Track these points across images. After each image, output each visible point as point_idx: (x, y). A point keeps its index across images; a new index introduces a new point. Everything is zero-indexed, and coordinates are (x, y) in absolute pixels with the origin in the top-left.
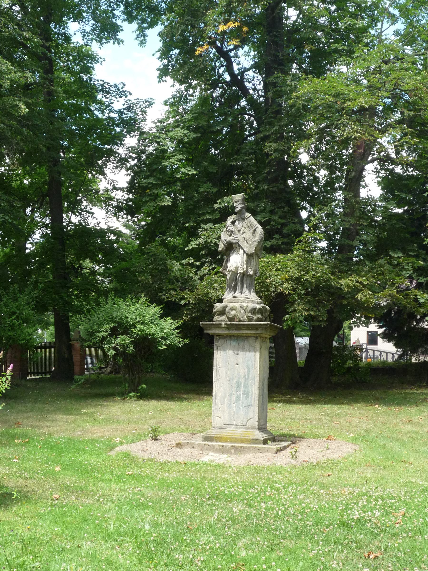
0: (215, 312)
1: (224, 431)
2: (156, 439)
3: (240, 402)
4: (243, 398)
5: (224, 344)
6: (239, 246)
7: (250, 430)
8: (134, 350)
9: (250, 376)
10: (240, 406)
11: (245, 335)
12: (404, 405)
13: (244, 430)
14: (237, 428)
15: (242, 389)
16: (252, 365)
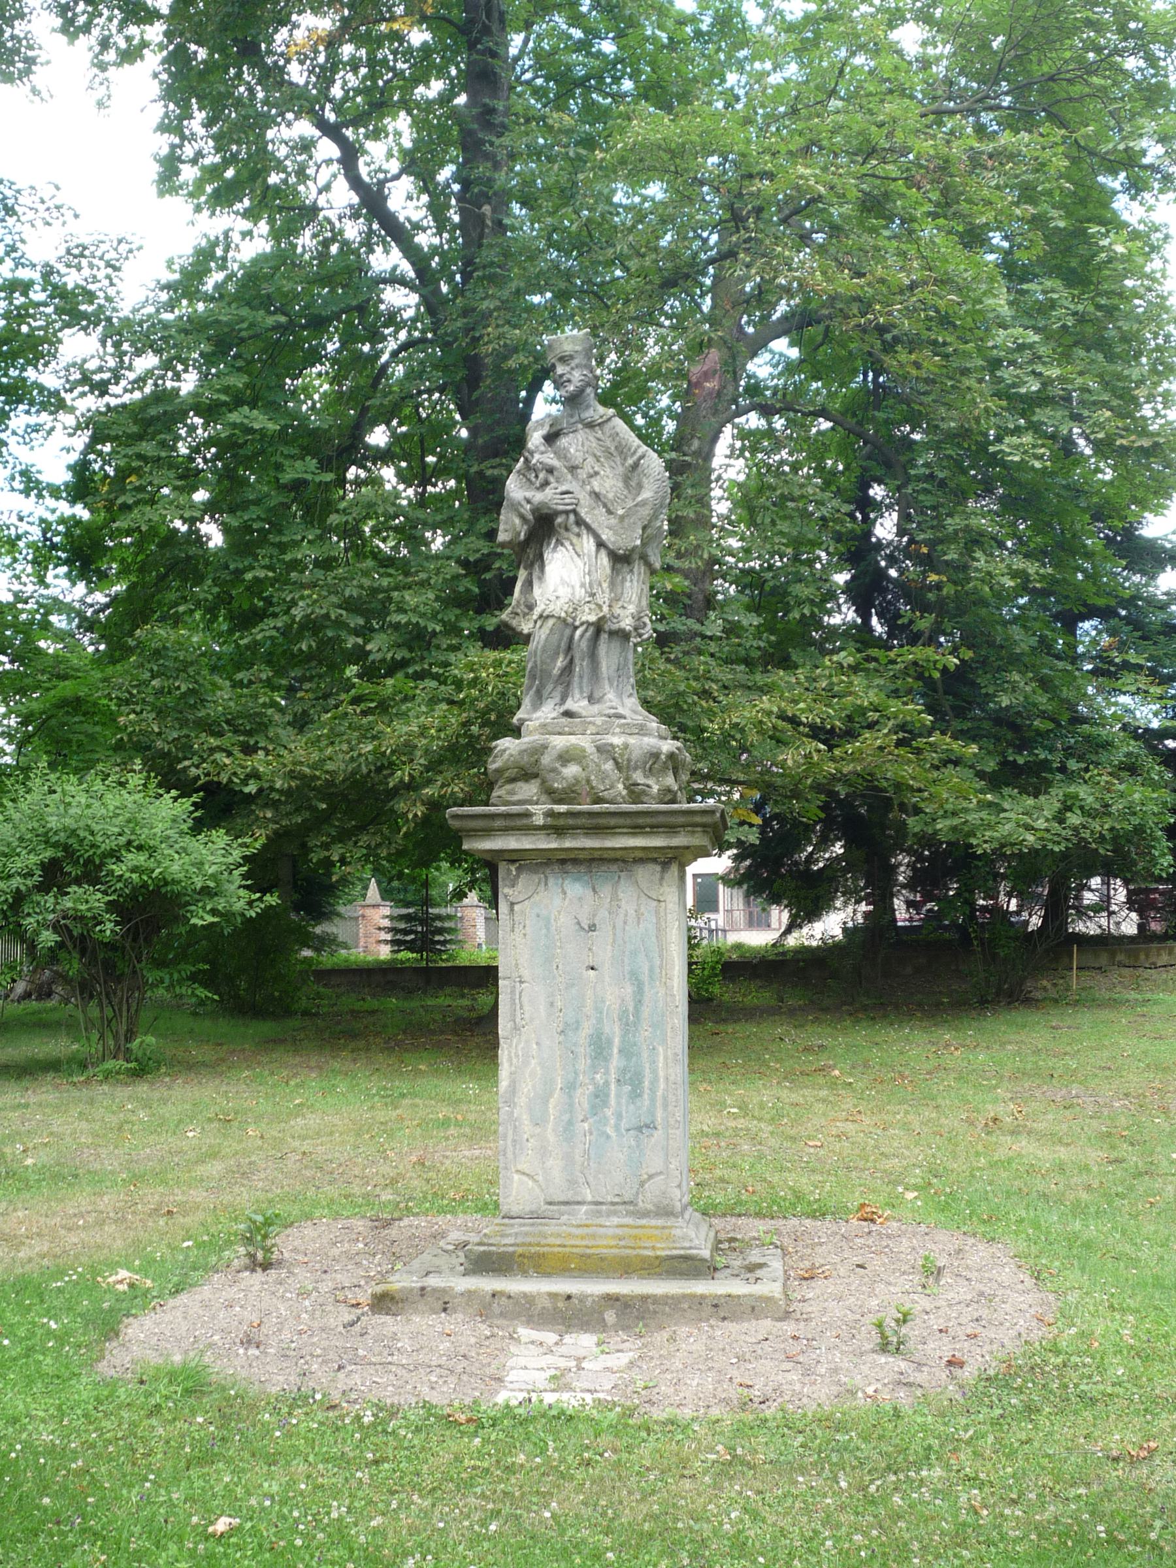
0: (499, 771)
1: (551, 1228)
2: (266, 1266)
3: (609, 1112)
4: (618, 1096)
5: (535, 892)
6: (580, 522)
7: (654, 1222)
8: (117, 929)
9: (646, 1011)
10: (609, 1131)
11: (619, 854)
13: (629, 1221)
14: (599, 1213)
15: (616, 1061)
16: (651, 970)
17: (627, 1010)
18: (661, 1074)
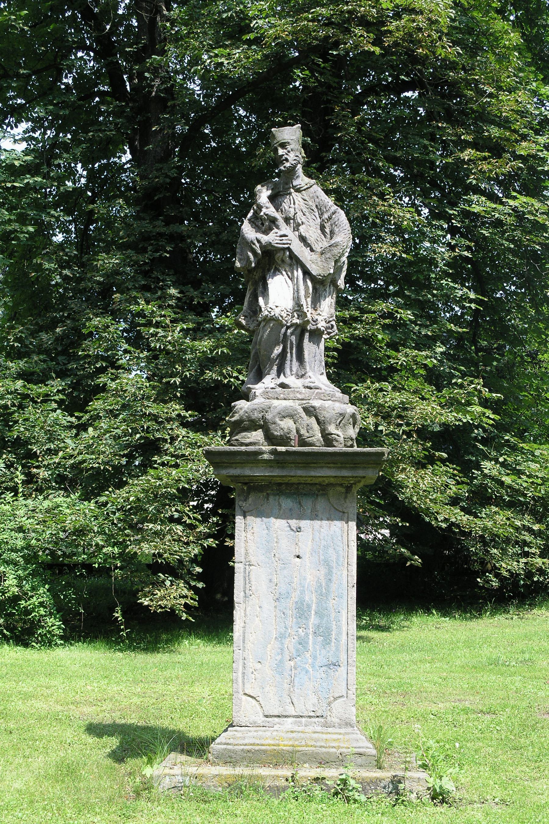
4: (314, 643)
12: (459, 608)
15: (313, 620)
16: (337, 559)
17: (321, 585)
18: (344, 628)
